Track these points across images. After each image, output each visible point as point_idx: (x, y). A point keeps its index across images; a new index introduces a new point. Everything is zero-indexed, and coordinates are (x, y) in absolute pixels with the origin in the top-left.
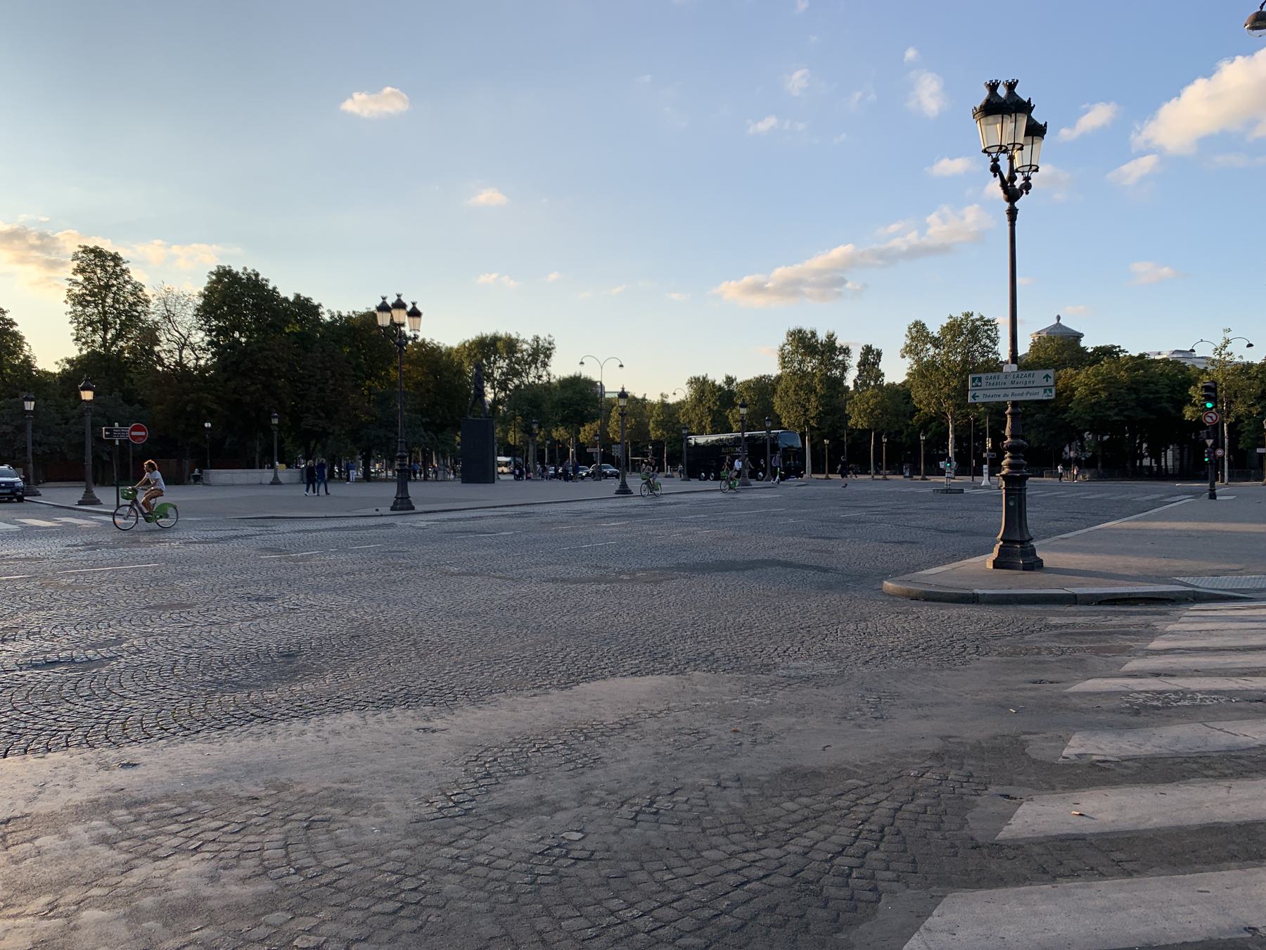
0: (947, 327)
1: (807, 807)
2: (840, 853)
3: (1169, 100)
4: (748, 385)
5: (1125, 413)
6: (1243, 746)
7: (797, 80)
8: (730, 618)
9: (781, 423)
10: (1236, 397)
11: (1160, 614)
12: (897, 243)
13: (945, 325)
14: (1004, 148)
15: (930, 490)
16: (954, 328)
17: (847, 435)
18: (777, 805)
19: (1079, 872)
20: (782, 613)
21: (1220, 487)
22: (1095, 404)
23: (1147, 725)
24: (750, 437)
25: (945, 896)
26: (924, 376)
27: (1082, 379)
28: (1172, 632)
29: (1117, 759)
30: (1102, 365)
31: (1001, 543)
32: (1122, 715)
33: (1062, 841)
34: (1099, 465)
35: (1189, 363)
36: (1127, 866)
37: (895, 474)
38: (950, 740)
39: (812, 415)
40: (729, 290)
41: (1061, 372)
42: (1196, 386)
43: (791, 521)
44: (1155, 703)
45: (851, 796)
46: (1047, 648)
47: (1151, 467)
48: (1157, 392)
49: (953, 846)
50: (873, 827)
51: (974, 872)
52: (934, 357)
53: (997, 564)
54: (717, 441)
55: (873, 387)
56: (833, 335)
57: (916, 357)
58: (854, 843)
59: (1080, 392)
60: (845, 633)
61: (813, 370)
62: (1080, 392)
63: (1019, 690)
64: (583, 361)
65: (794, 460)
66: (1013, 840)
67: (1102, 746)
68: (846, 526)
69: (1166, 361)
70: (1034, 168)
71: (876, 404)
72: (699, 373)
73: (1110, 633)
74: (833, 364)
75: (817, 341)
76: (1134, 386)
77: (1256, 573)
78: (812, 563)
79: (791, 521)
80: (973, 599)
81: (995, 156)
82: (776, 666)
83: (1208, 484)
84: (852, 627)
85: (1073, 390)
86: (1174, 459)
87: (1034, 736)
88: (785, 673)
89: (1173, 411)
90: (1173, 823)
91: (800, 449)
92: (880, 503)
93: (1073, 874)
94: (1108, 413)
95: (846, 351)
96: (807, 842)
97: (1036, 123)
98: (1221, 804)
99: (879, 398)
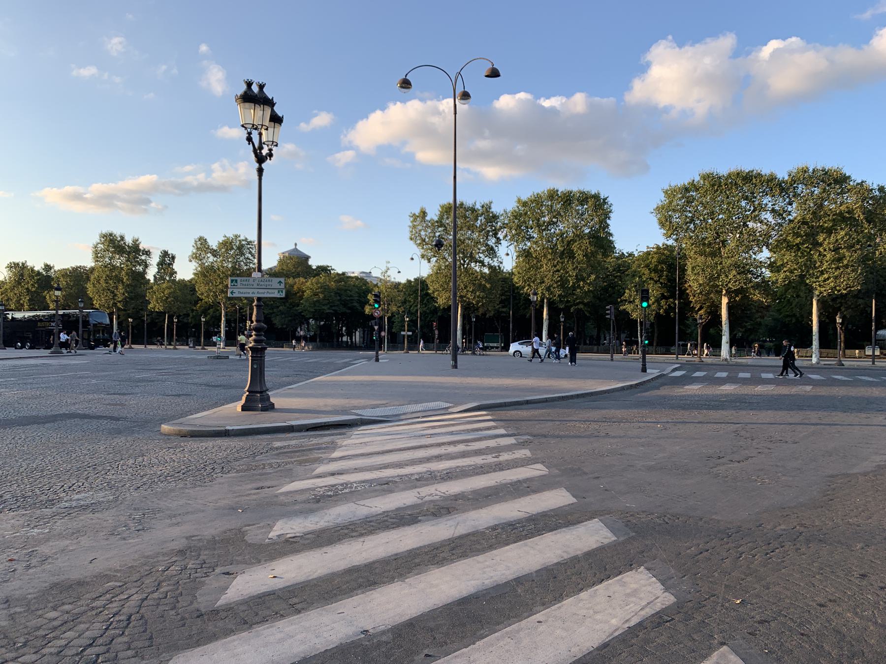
0: (222, 243)
1: (67, 613)
2: (91, 645)
3: (362, 119)
4: (65, 273)
5: (333, 308)
6: (374, 514)
7: (115, 44)
8: (24, 464)
9: (93, 304)
10: (392, 301)
11: (340, 434)
12: (189, 179)
13: (221, 242)
14: (255, 127)
15: (205, 357)
16: (227, 244)
17: (147, 315)
18: (40, 616)
19: (267, 618)
20: (74, 456)
21: (382, 354)
22: (316, 301)
23: (322, 508)
24: (63, 315)
25: (171, 659)
26: (205, 276)
27: (308, 286)
28: (345, 446)
29: (302, 534)
30: (321, 277)
31: (247, 393)
32: (309, 504)
33: (260, 598)
34: (318, 340)
35: (369, 280)
36: (299, 606)
37: (182, 345)
38: (193, 538)
39: (120, 300)
40: (52, 195)
41: (297, 280)
42: (371, 293)
43: (94, 381)
44: (329, 493)
45: (108, 596)
46: (269, 464)
47: (347, 342)
48: (351, 296)
49: (183, 619)
50: (122, 618)
51: (195, 635)
52: (212, 263)
53: (244, 408)
54: (33, 316)
55: (168, 281)
56: (137, 240)
57: (200, 262)
58: (105, 633)
59: (308, 293)
60: (124, 467)
61: (120, 265)
62: (308, 293)
63: (246, 495)
64: (413, 257)
65: (103, 334)
66: (227, 605)
67: (294, 527)
68: (139, 384)
69: (357, 278)
70: (275, 144)
71: (170, 293)
72: (19, 260)
73: (310, 450)
74: (138, 261)
75: (125, 243)
76: (339, 292)
77: (394, 406)
78: (107, 414)
79: (94, 381)
80: (226, 434)
81: (250, 129)
82: (60, 500)
83: (375, 353)
84: (131, 461)
85: (303, 292)
86: (360, 337)
87: (251, 527)
88: (67, 505)
89: (360, 308)
90: (329, 571)
91: (108, 325)
92: (167, 367)
93: (264, 620)
94: (324, 307)
95: (147, 253)
96: (63, 642)
97: (276, 115)
98: (357, 553)
99: (172, 290)
